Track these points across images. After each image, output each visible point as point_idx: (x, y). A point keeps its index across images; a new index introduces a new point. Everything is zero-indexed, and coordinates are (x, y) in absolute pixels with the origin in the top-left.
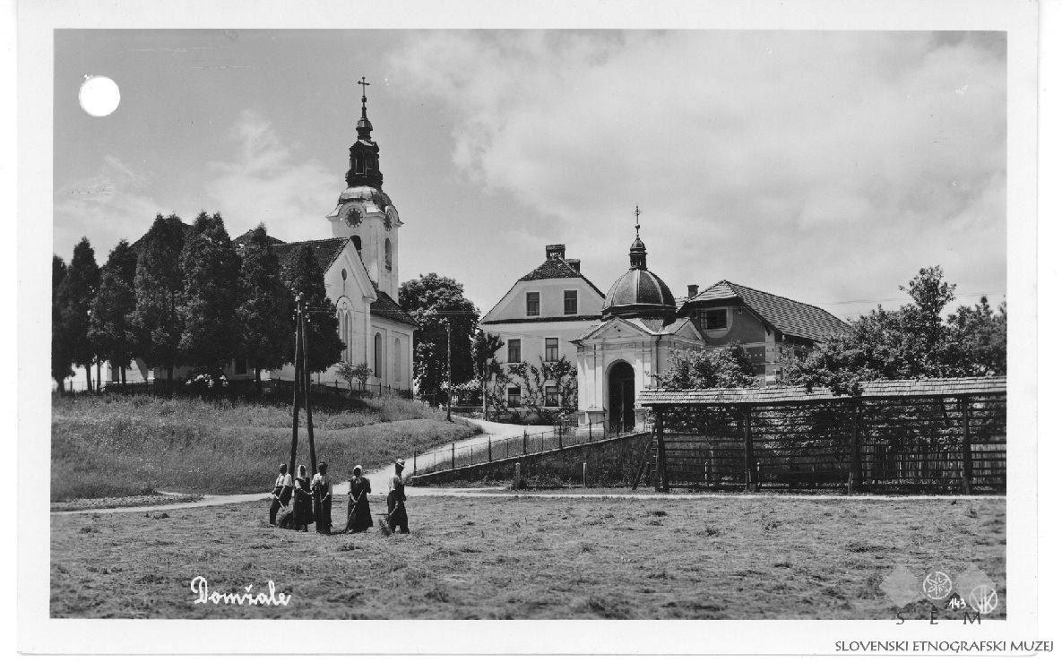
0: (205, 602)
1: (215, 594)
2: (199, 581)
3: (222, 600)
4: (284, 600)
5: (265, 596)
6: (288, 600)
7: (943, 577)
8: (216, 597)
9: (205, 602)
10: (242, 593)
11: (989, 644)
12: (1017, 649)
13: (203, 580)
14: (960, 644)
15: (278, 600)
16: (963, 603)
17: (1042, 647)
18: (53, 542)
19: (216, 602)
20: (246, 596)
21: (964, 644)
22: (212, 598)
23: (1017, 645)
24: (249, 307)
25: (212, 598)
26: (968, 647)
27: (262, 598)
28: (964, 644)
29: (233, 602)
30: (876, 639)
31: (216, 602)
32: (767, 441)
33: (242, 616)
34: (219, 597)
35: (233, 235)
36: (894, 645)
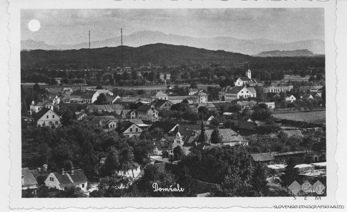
0: (157, 191)
1: (160, 188)
2: (154, 184)
3: (163, 190)
4: (182, 190)
5: (176, 189)
6: (183, 190)
7: (308, 185)
8: (160, 189)
9: (157, 191)
10: (169, 188)
11: (324, 206)
12: (332, 208)
13: (156, 184)
14: (314, 206)
15: (180, 190)
16: (143, 18)
17: (341, 207)
18: (23, 159)
19: (161, 191)
20: (170, 189)
21: (315, 206)
22: (159, 189)
23: (332, 206)
24: (87, 69)
25: (159, 189)
26: (317, 207)
27: (175, 189)
28: (315, 206)
29: (166, 191)
30: (287, 205)
31: (161, 191)
32: (311, 190)
33: (57, 196)
34: (161, 189)
35: (295, 182)
36: (293, 206)
